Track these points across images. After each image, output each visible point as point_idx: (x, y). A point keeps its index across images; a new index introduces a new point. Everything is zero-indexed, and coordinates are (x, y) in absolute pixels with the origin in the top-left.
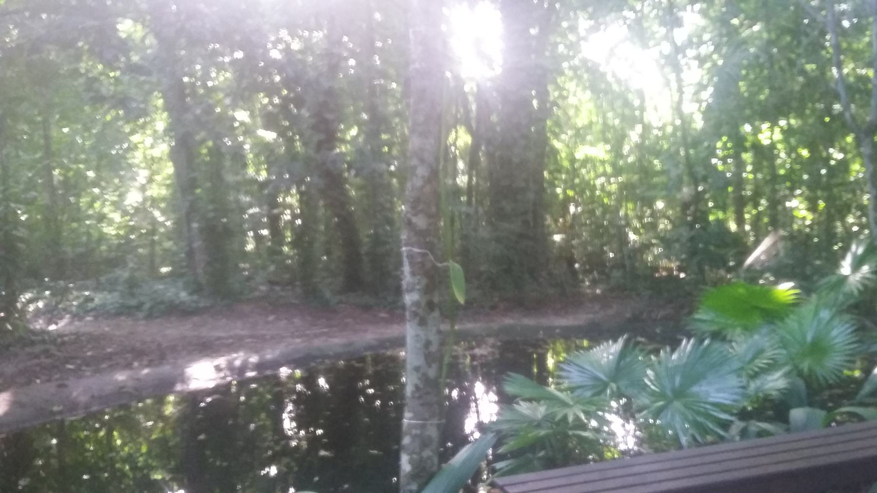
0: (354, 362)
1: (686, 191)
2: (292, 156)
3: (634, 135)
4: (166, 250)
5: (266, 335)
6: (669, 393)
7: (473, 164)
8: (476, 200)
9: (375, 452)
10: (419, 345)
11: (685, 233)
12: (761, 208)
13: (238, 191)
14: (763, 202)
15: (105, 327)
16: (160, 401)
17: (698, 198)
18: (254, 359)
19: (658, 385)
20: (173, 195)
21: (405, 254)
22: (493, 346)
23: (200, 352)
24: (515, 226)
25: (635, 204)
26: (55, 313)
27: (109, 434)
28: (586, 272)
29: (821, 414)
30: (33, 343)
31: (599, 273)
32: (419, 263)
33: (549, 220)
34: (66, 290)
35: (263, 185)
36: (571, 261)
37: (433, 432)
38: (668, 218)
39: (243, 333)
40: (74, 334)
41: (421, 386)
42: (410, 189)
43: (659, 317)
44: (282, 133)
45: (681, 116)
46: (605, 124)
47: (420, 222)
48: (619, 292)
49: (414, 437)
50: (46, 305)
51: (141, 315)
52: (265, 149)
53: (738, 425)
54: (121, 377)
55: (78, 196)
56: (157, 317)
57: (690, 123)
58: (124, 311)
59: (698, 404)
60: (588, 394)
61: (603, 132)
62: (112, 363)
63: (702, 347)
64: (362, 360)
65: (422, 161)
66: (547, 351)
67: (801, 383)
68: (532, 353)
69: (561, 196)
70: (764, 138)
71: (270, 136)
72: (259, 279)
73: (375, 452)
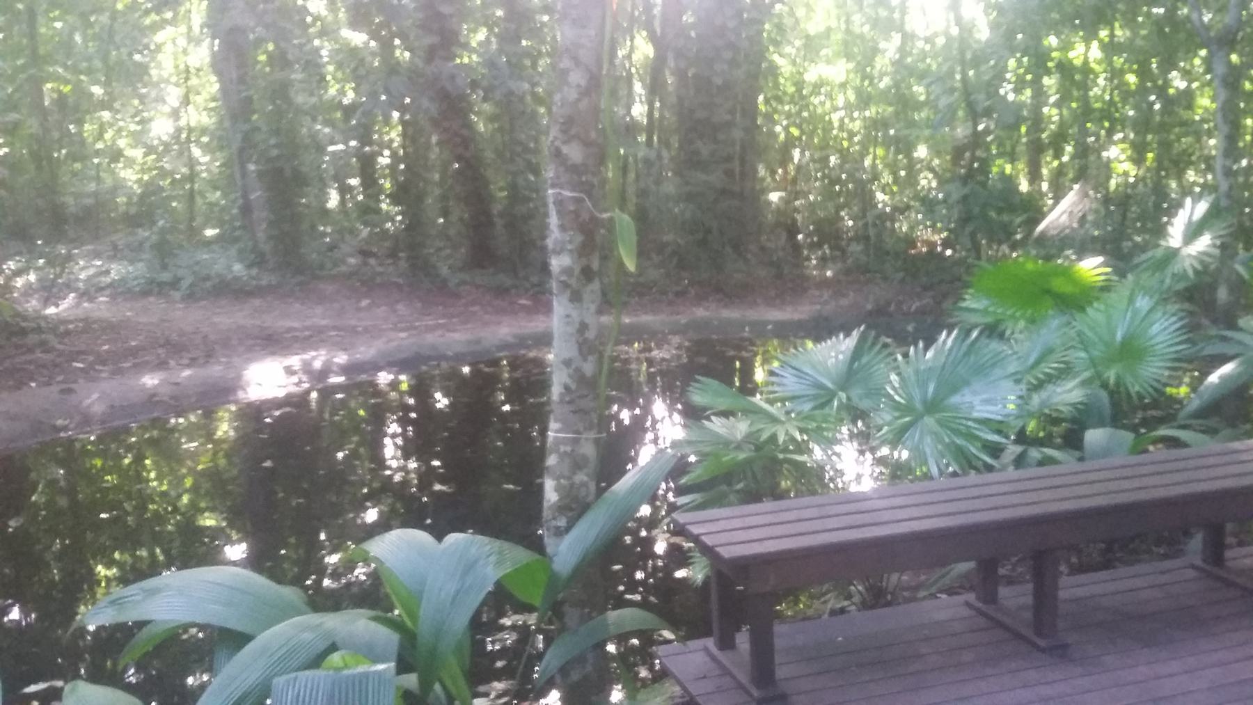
0: (482, 366)
1: (961, 131)
2: (392, 68)
3: (890, 47)
4: (211, 205)
5: (357, 326)
6: (918, 405)
7: (655, 88)
8: (659, 138)
9: (511, 487)
10: (571, 329)
11: (957, 192)
12: (1065, 159)
13: (314, 120)
14: (1069, 149)
15: (127, 311)
16: (209, 414)
17: (976, 140)
18: (341, 359)
19: (904, 395)
20: (221, 122)
21: (551, 200)
22: (679, 348)
23: (264, 348)
24: (715, 178)
25: (887, 150)
26: (55, 290)
27: (139, 459)
28: (814, 246)
29: (1128, 437)
30: (23, 332)
31: (831, 248)
32: (571, 212)
33: (762, 171)
34: (69, 258)
35: (349, 111)
36: (792, 230)
37: (588, 450)
38: (932, 170)
39: (324, 322)
40: (81, 320)
41: (573, 387)
42: (559, 104)
43: (914, 308)
44: (374, 35)
45: (959, 21)
46: (848, 31)
47: (574, 153)
48: (857, 275)
49: (563, 456)
50: (39, 280)
51: (177, 295)
52: (351, 60)
53: (1013, 450)
54: (150, 380)
55: (80, 122)
56: (202, 299)
57: (970, 31)
58: (153, 288)
59: (958, 421)
60: (807, 407)
61: (846, 43)
62: (136, 361)
63: (969, 341)
64: (495, 363)
65: (577, 61)
66: (756, 354)
67: (1104, 395)
68: (733, 359)
69: (782, 137)
70: (1077, 55)
71: (358, 38)
72: (345, 248)
73: (511, 487)
